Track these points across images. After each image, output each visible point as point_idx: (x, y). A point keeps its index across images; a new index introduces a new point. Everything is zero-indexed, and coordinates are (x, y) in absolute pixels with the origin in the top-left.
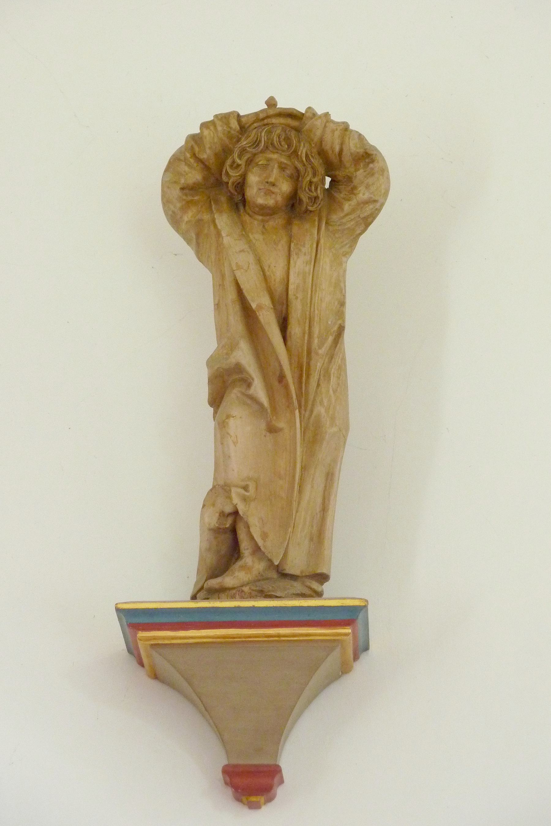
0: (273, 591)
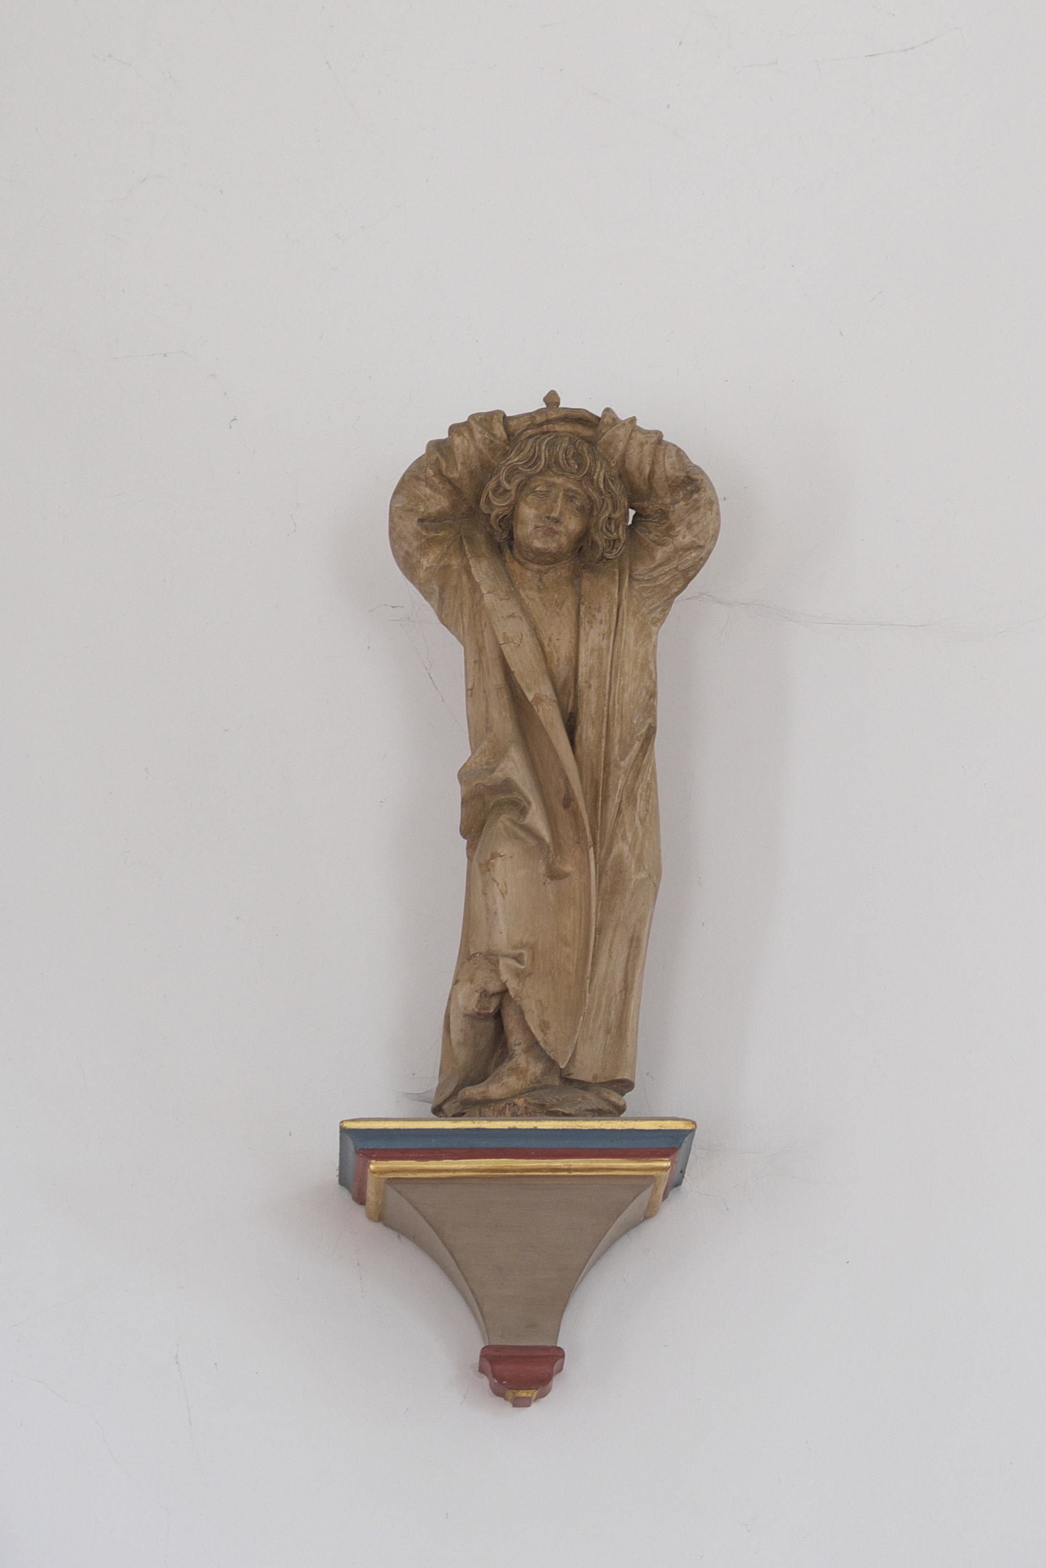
0: (558, 1105)
